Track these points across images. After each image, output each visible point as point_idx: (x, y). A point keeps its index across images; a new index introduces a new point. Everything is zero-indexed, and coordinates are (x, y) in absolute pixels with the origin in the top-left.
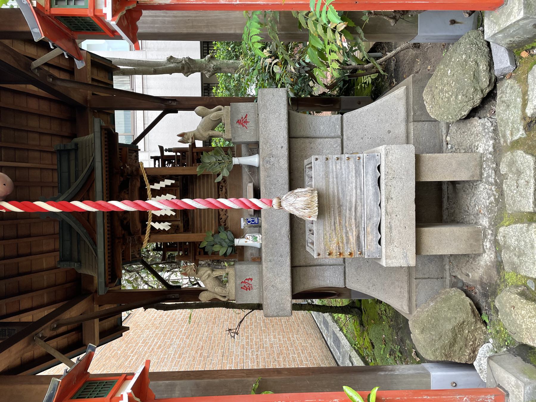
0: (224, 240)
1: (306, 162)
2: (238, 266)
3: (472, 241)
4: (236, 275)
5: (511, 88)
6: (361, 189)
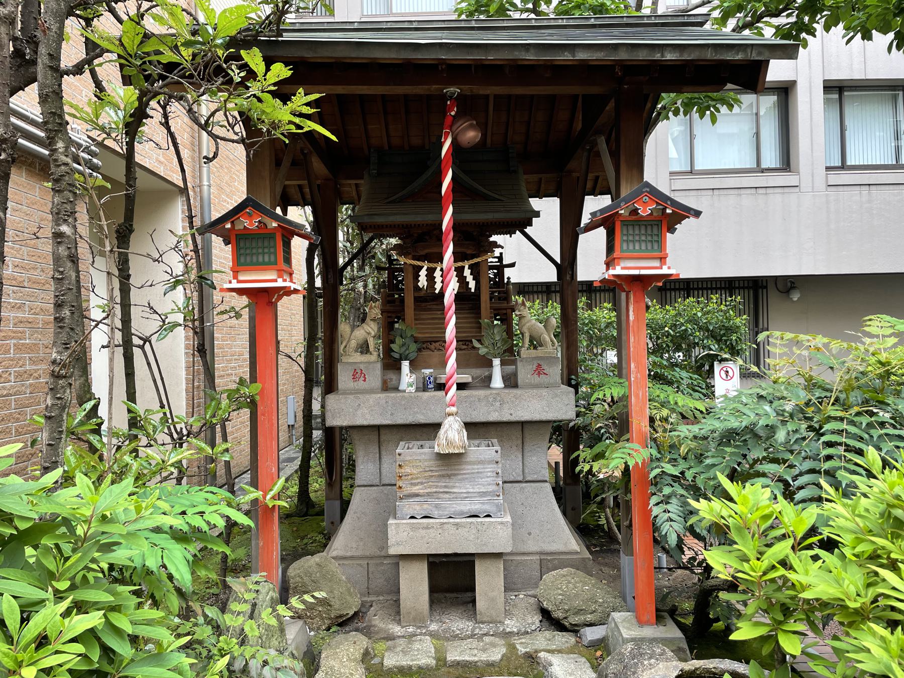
0: (407, 349)
1: (495, 441)
2: (379, 366)
3: (413, 613)
4: (369, 363)
5: (567, 642)
6: (466, 497)
